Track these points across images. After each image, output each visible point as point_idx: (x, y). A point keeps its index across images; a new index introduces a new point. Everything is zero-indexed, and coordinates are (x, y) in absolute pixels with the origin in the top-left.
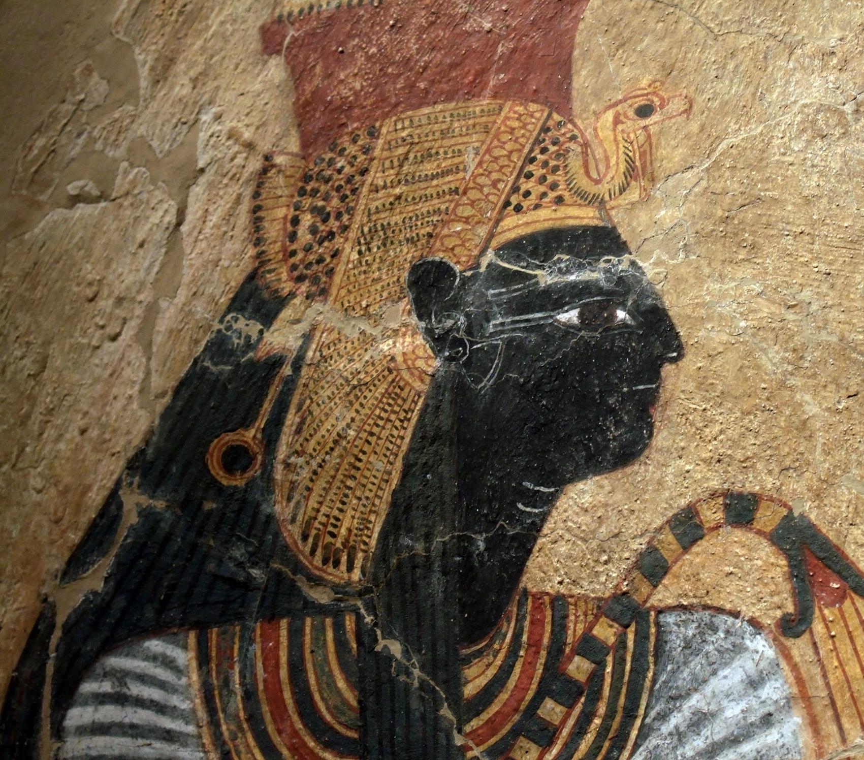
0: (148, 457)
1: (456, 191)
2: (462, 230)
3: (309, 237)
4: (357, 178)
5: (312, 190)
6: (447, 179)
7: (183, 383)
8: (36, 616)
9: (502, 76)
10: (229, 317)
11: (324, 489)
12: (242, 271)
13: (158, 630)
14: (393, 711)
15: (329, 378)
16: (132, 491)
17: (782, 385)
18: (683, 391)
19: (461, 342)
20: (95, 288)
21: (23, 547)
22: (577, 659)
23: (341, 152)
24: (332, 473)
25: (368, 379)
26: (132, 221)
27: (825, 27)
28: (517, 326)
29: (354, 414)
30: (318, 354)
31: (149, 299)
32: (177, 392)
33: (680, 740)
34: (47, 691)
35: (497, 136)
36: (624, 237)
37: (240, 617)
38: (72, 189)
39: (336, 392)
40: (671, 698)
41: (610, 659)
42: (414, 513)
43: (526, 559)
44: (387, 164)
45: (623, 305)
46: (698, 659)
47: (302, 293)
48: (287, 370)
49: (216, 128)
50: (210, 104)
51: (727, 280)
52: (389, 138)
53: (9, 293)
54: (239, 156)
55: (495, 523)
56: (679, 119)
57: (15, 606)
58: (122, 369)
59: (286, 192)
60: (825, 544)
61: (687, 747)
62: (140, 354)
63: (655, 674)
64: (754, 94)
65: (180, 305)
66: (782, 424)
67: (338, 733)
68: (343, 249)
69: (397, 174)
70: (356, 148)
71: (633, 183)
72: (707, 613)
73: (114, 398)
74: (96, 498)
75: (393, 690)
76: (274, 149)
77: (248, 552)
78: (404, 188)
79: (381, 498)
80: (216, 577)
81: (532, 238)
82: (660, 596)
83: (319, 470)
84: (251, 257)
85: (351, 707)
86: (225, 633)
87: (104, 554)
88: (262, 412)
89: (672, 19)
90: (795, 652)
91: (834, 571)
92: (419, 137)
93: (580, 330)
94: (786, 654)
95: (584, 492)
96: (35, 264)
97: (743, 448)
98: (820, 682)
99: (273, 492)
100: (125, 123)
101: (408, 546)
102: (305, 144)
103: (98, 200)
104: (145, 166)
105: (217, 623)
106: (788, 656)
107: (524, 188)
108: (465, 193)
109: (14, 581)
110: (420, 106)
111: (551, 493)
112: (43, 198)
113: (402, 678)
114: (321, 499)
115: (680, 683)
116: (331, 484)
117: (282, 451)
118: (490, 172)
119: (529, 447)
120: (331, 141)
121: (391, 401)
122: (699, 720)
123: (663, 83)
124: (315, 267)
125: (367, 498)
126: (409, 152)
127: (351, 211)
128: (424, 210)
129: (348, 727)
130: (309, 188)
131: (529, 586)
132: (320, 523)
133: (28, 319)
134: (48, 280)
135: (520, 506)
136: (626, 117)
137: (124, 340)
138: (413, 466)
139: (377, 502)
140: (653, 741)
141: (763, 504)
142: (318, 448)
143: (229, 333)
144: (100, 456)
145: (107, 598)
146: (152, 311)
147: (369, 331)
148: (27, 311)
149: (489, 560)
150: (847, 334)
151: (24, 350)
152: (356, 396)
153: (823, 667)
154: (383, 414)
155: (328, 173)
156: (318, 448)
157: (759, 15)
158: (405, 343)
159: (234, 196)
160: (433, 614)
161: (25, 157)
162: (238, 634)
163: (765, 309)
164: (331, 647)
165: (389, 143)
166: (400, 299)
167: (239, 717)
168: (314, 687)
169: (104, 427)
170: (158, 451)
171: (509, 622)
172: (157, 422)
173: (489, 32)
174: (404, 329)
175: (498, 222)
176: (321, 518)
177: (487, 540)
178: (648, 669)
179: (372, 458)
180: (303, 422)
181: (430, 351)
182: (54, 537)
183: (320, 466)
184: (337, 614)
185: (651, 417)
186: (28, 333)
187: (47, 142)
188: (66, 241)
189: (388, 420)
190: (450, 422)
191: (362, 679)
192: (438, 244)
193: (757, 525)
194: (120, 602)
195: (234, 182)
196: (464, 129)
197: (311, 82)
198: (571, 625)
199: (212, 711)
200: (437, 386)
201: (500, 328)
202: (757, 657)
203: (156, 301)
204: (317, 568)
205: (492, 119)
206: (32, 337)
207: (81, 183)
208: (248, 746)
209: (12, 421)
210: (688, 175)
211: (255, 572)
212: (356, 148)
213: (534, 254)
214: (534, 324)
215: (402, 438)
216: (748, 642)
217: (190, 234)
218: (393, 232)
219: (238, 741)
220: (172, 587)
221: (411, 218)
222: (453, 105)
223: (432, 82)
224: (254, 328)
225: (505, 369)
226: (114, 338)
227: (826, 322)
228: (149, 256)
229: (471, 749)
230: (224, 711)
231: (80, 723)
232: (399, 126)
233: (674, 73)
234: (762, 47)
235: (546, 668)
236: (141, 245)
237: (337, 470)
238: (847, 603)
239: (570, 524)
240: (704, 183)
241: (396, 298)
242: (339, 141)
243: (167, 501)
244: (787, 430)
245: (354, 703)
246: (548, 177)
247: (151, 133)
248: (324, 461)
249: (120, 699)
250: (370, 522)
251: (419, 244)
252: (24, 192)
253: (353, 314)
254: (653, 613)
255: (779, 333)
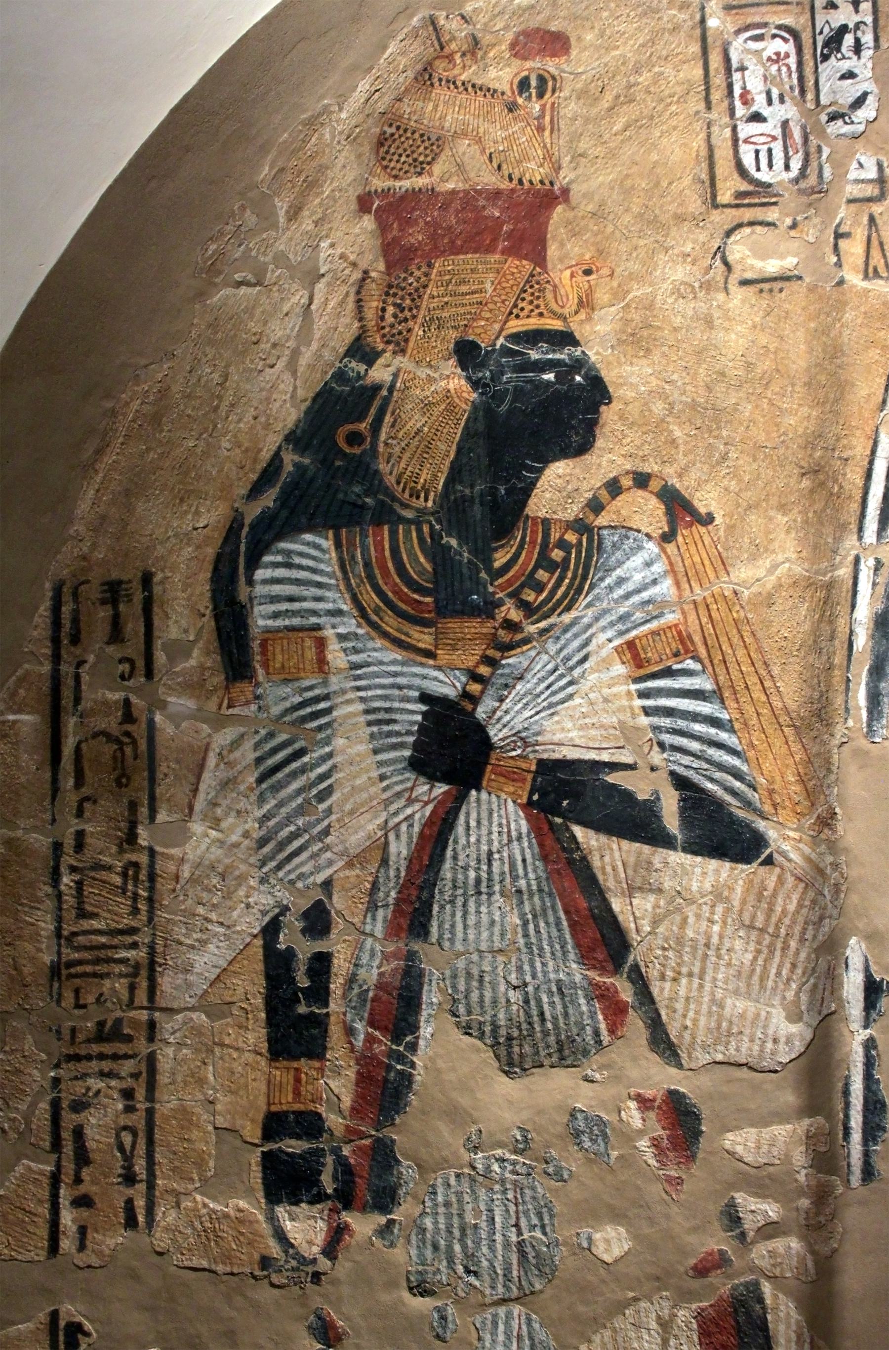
7: (318, 395)
13: (310, 529)
17: (663, 420)
19: (488, 385)
32: (314, 399)
35: (504, 275)
37: (358, 523)
38: (238, 277)
48: (385, 392)
49: (330, 251)
60: (683, 498)
73: (277, 399)
74: (266, 455)
80: (343, 502)
81: (526, 333)
87: (274, 486)
94: (664, 550)
102: (389, 266)
103: (255, 285)
105: (346, 526)
106: (665, 552)
110: (458, 254)
117: (383, 436)
122: (621, 581)
133: (213, 351)
140: (596, 591)
146: (296, 354)
158: (454, 381)
163: (654, 382)
164: (415, 541)
169: (269, 417)
170: (304, 431)
175: (505, 323)
180: (395, 421)
184: (418, 524)
186: (214, 359)
191: (434, 558)
194: (284, 513)
200: (475, 407)
210: (612, 309)
211: (368, 500)
213: (527, 342)
224: (362, 368)
225: (514, 400)
226: (272, 366)
244: (665, 443)
249: (289, 565)
255: (663, 396)
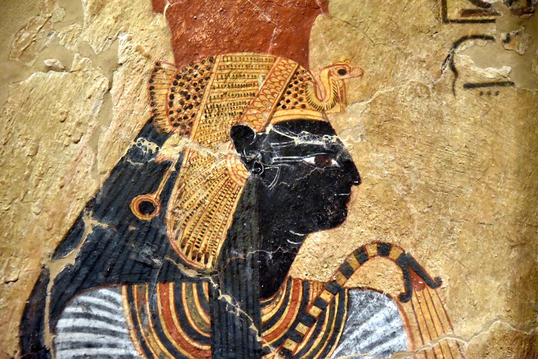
0: (97, 202)
1: (254, 95)
2: (257, 113)
3: (179, 105)
4: (204, 81)
5: (181, 83)
6: (249, 88)
7: (116, 169)
8: (39, 274)
9: (276, 44)
10: (139, 139)
11: (193, 225)
12: (145, 117)
13: (106, 284)
14: (227, 326)
15: (194, 175)
16: (89, 218)
17: (402, 200)
18: (361, 198)
19: (259, 165)
20: (64, 116)
21: (29, 241)
22: (314, 307)
23: (196, 67)
24: (197, 218)
25: (215, 177)
26: (83, 84)
27: (421, 49)
28: (285, 161)
29: (208, 193)
30: (188, 163)
31: (95, 125)
32: (112, 172)
33: (358, 342)
34: (47, 311)
35: (274, 71)
36: (334, 127)
37: (148, 280)
39: (198, 182)
40: (354, 325)
41: (328, 308)
42: (238, 240)
43: (291, 264)
44: (219, 76)
45: (335, 158)
46: (365, 309)
47: (177, 132)
48: (173, 169)
50: (125, 32)
51: (379, 153)
52: (220, 64)
53: (13, 112)
54: (142, 60)
55: (277, 247)
56: (358, 78)
57: (25, 269)
58: (82, 158)
59: (167, 82)
61: (361, 344)
62: (91, 152)
63: (347, 315)
64: (390, 73)
65: (113, 130)
66: (402, 216)
67: (200, 334)
68: (197, 114)
69: (225, 82)
70: (203, 66)
71: (337, 104)
72: (369, 291)
74: (70, 220)
75: (226, 316)
76: (161, 60)
77: (153, 251)
78: (228, 89)
79: (222, 232)
81: (291, 122)
82: (350, 283)
83: (190, 217)
84: (149, 111)
85: (206, 324)
86: (141, 287)
88: (160, 187)
89: (354, 33)
90: (405, 308)
91: (420, 277)
92: (235, 66)
93: (315, 167)
95: (317, 237)
96: (28, 99)
97: (386, 224)
98: (414, 320)
99: (166, 225)
100: (76, 33)
101: (235, 254)
103: (63, 70)
104: (89, 57)
107: (287, 98)
108: (258, 96)
109: (24, 257)
110: (235, 51)
111: (302, 236)
112: (29, 64)
113: (231, 312)
114: (191, 230)
115: (358, 319)
116: (196, 224)
118: (270, 89)
119: (292, 215)
120: (190, 61)
121: (226, 189)
122: (366, 334)
123: (350, 61)
124: (183, 120)
125: (215, 232)
126: (229, 73)
127: (201, 96)
128: (238, 101)
129: (205, 332)
130: (179, 82)
131: (293, 276)
132: (191, 241)
134: (36, 108)
135: (288, 241)
136: (334, 73)
137: (82, 144)
138: (238, 219)
139: (220, 233)
140: (346, 342)
141: (393, 248)
142: (190, 207)
143: (140, 147)
144: (70, 199)
145: (77, 268)
146: (96, 132)
147: (212, 154)
148: (25, 123)
149: (274, 263)
150: (428, 181)
151: (24, 142)
152: (209, 184)
153: (416, 315)
154: (222, 194)
155: (189, 76)
156: (190, 207)
157: (393, 39)
158: (230, 160)
159: (139, 80)
160: (246, 285)
161: (17, 41)
162: (147, 288)
163: (396, 167)
165: (220, 67)
166: (227, 141)
167: (149, 326)
168: (188, 314)
169: (73, 186)
170: (102, 200)
171: (283, 290)
172: (101, 186)
173: (270, 22)
174: (229, 156)
175: (274, 112)
176: (191, 239)
177: (273, 254)
178: (344, 313)
179: (218, 214)
180: (181, 193)
181: (244, 168)
182: (47, 237)
183: (191, 215)
184: (199, 282)
185: (346, 207)
187: (30, 36)
188: (45, 89)
189: (225, 197)
190: (255, 201)
192: (245, 118)
193: (391, 256)
194: (84, 271)
195: (139, 73)
196: (257, 66)
197: (180, 30)
198: (311, 293)
199: (135, 322)
200: (249, 185)
201: (277, 161)
202: (390, 310)
203: (99, 127)
204: (189, 261)
205: (271, 63)
206: (29, 136)
207: (53, 60)
208: (154, 339)
209: (19, 178)
210: (362, 104)
211: (156, 261)
212: (203, 66)
213: (292, 129)
214: (293, 161)
215: (232, 206)
216: (386, 303)
217: (115, 95)
218: (222, 109)
219: (149, 337)
220: (113, 265)
221: (231, 104)
222: (252, 54)
223: (241, 42)
224: (153, 146)
226: (76, 142)
227: (420, 175)
228: (94, 104)
229: (265, 343)
230: (142, 323)
231: (66, 326)
232: (225, 59)
233: (355, 57)
234: (394, 53)
235: (300, 310)
236: (89, 98)
237: (200, 218)
238: (425, 290)
239: (311, 250)
240: (369, 109)
241: (225, 140)
242: (195, 62)
243: (109, 224)
244: (404, 218)
245: (208, 321)
246: (298, 95)
247: (91, 41)
248: (192, 213)
249: (88, 316)
250: (217, 242)
251: (235, 116)
252: (17, 59)
253: (203, 145)
254: (346, 290)
